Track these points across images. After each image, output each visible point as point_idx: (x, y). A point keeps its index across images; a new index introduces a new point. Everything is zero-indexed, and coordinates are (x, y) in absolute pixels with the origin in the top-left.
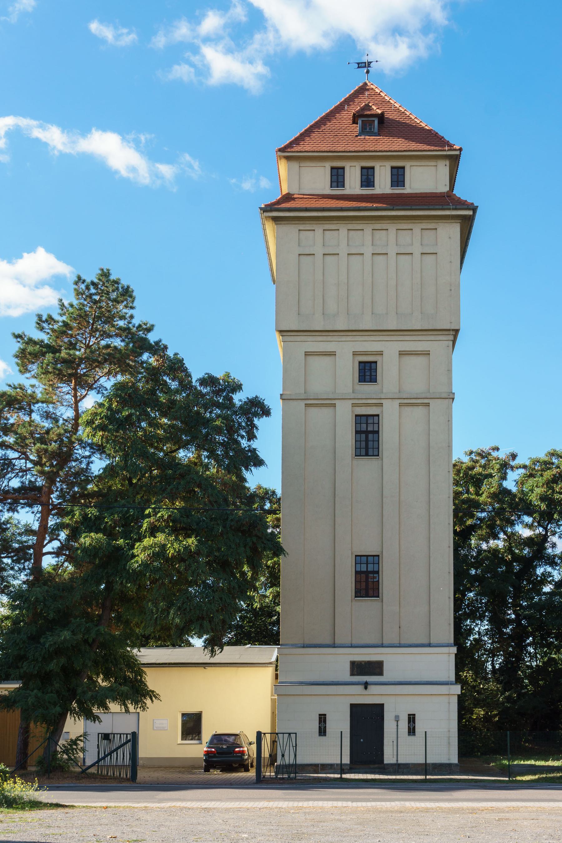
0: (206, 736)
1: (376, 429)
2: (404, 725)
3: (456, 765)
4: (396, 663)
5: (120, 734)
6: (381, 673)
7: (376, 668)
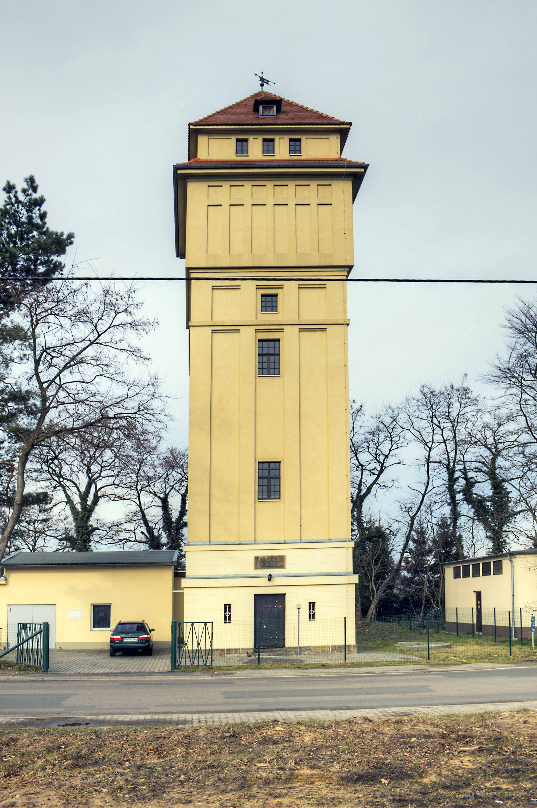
0: (114, 624)
1: (277, 352)
2: (305, 612)
3: (354, 646)
4: (296, 560)
5: (35, 624)
6: (283, 566)
7: (276, 562)
